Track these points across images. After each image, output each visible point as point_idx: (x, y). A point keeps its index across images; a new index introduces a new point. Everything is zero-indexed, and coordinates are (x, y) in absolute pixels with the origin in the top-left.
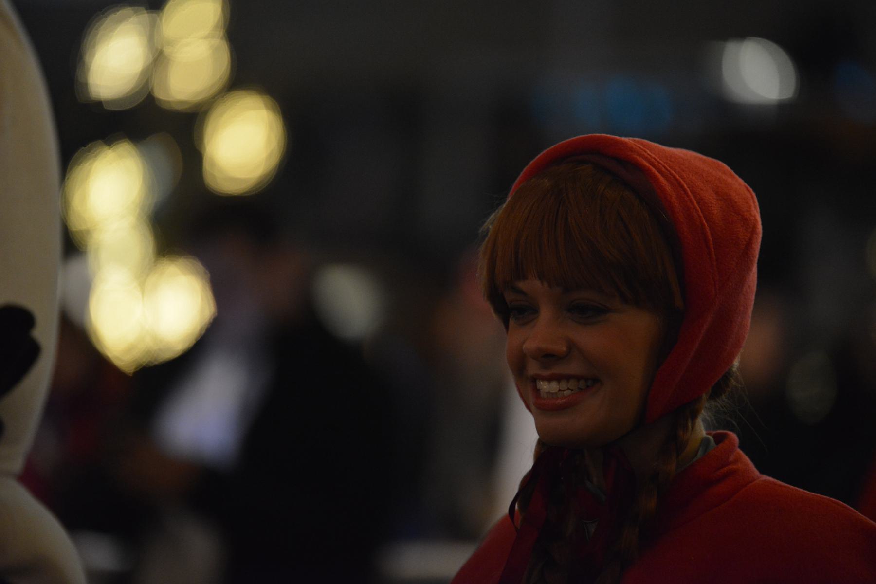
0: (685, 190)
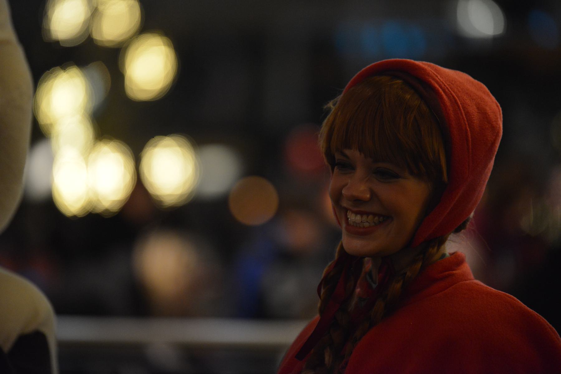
0: (459, 106)
